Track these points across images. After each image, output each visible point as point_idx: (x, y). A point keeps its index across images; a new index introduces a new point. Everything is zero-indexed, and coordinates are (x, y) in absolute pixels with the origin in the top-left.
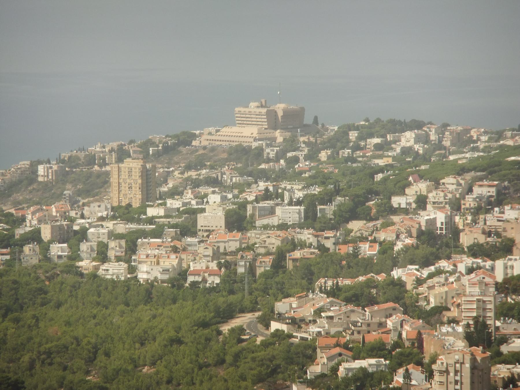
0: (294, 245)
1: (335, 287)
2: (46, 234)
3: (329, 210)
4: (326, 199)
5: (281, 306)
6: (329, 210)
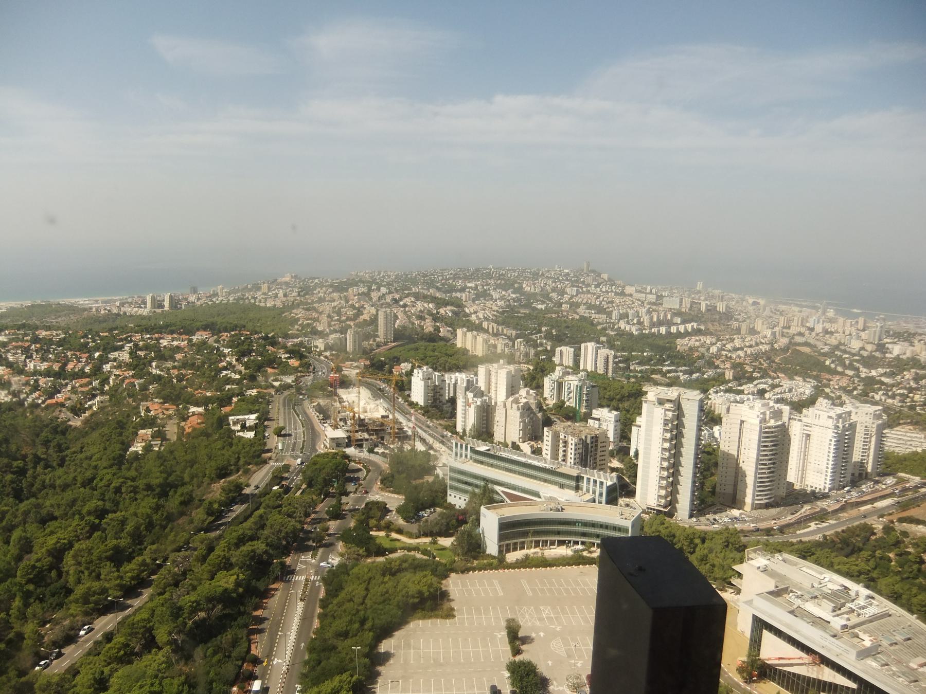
0: (296, 300)
1: (43, 406)
2: (250, 297)
3: (302, 293)
4: (302, 291)
5: (293, 311)
6: (302, 293)
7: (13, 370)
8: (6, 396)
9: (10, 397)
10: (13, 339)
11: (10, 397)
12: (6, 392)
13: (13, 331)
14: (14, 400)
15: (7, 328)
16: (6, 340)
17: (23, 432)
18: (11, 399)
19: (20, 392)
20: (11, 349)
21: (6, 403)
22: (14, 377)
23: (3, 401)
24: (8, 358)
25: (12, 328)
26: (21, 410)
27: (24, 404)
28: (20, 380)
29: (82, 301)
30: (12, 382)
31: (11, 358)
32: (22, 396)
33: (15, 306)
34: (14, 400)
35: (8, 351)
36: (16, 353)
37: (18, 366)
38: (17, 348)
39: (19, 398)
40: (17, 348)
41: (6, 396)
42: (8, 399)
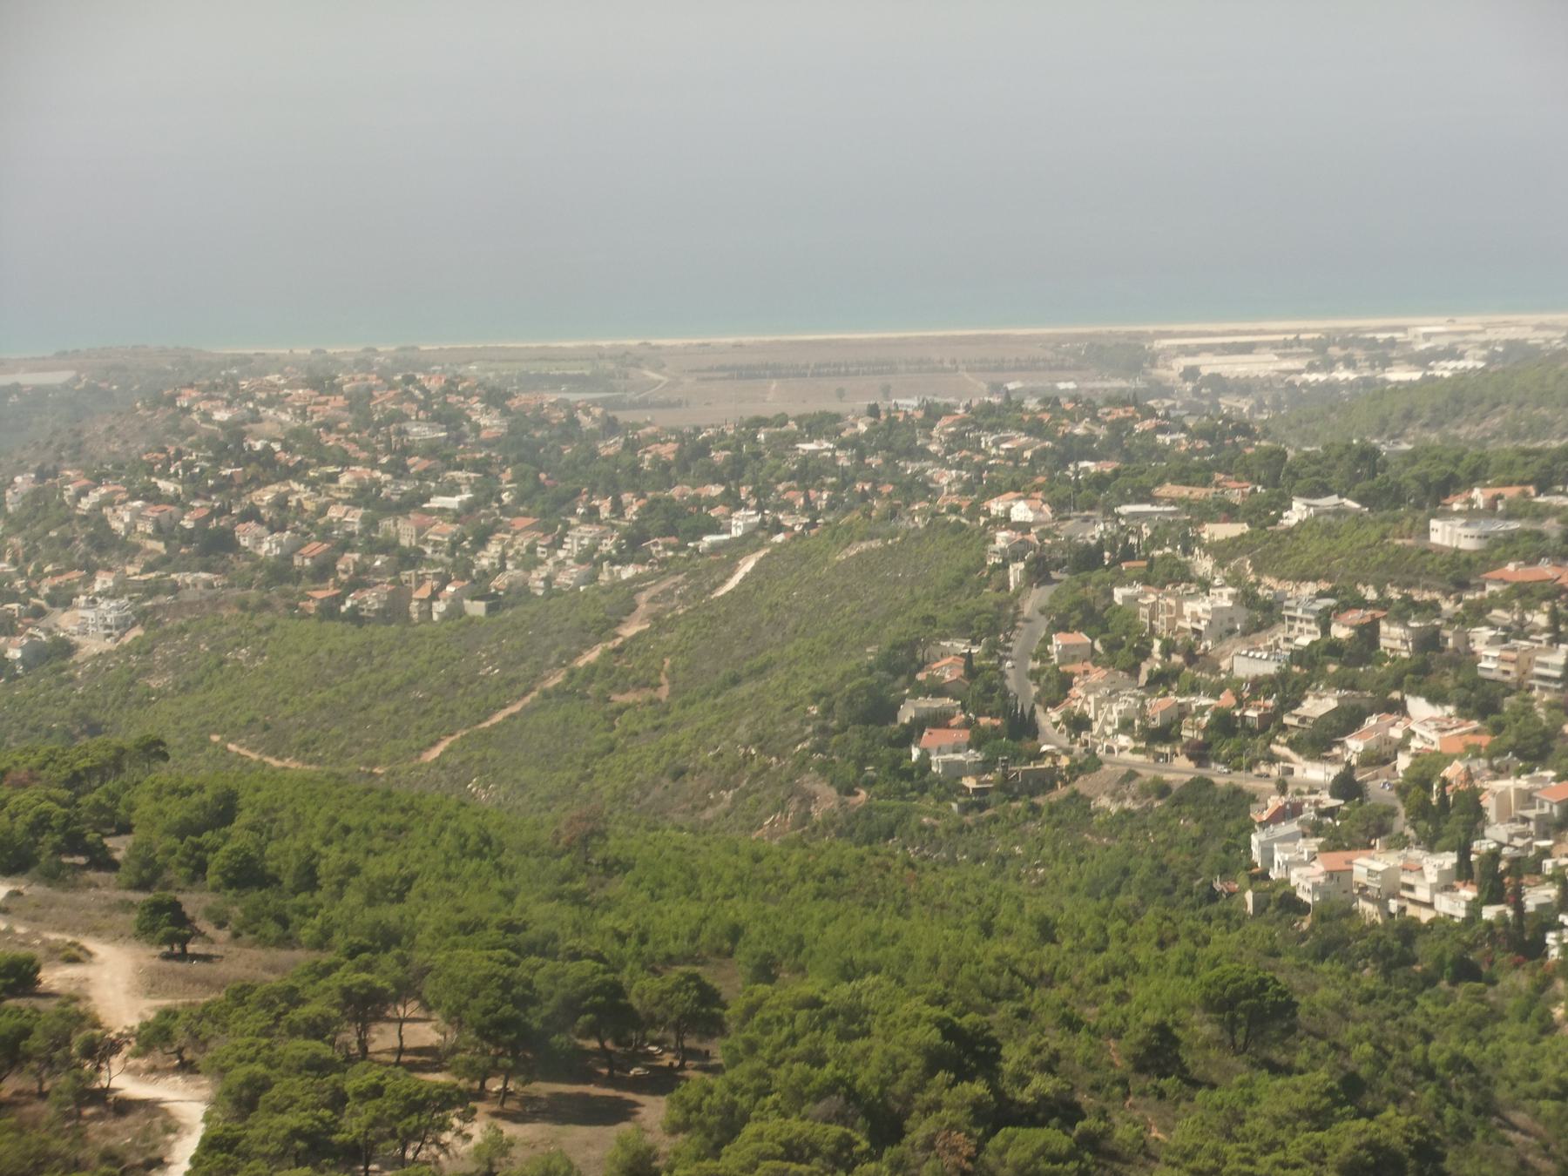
7: (1498, 728)
8: (1446, 886)
9: (1468, 893)
10: (1511, 538)
11: (1468, 893)
12: (1449, 860)
13: (1511, 492)
14: (1489, 913)
15: (1476, 476)
16: (1468, 544)
17: (1519, 1118)
18: (1474, 908)
19: (1527, 867)
20: (1494, 602)
21: (1442, 925)
22: (1499, 772)
23: (1425, 916)
24: (1473, 658)
25: (1507, 472)
26: (1522, 980)
27: (1540, 949)
28: (1527, 798)
29: (1426, 329)
30: (1488, 802)
31: (1490, 658)
32: (1538, 896)
33: (1535, 338)
34: (1489, 913)
35: (1477, 614)
36: (1520, 631)
37: (1527, 710)
38: (1525, 594)
39: (1519, 907)
40: (1525, 594)
41: (1446, 886)
42: (1454, 905)
